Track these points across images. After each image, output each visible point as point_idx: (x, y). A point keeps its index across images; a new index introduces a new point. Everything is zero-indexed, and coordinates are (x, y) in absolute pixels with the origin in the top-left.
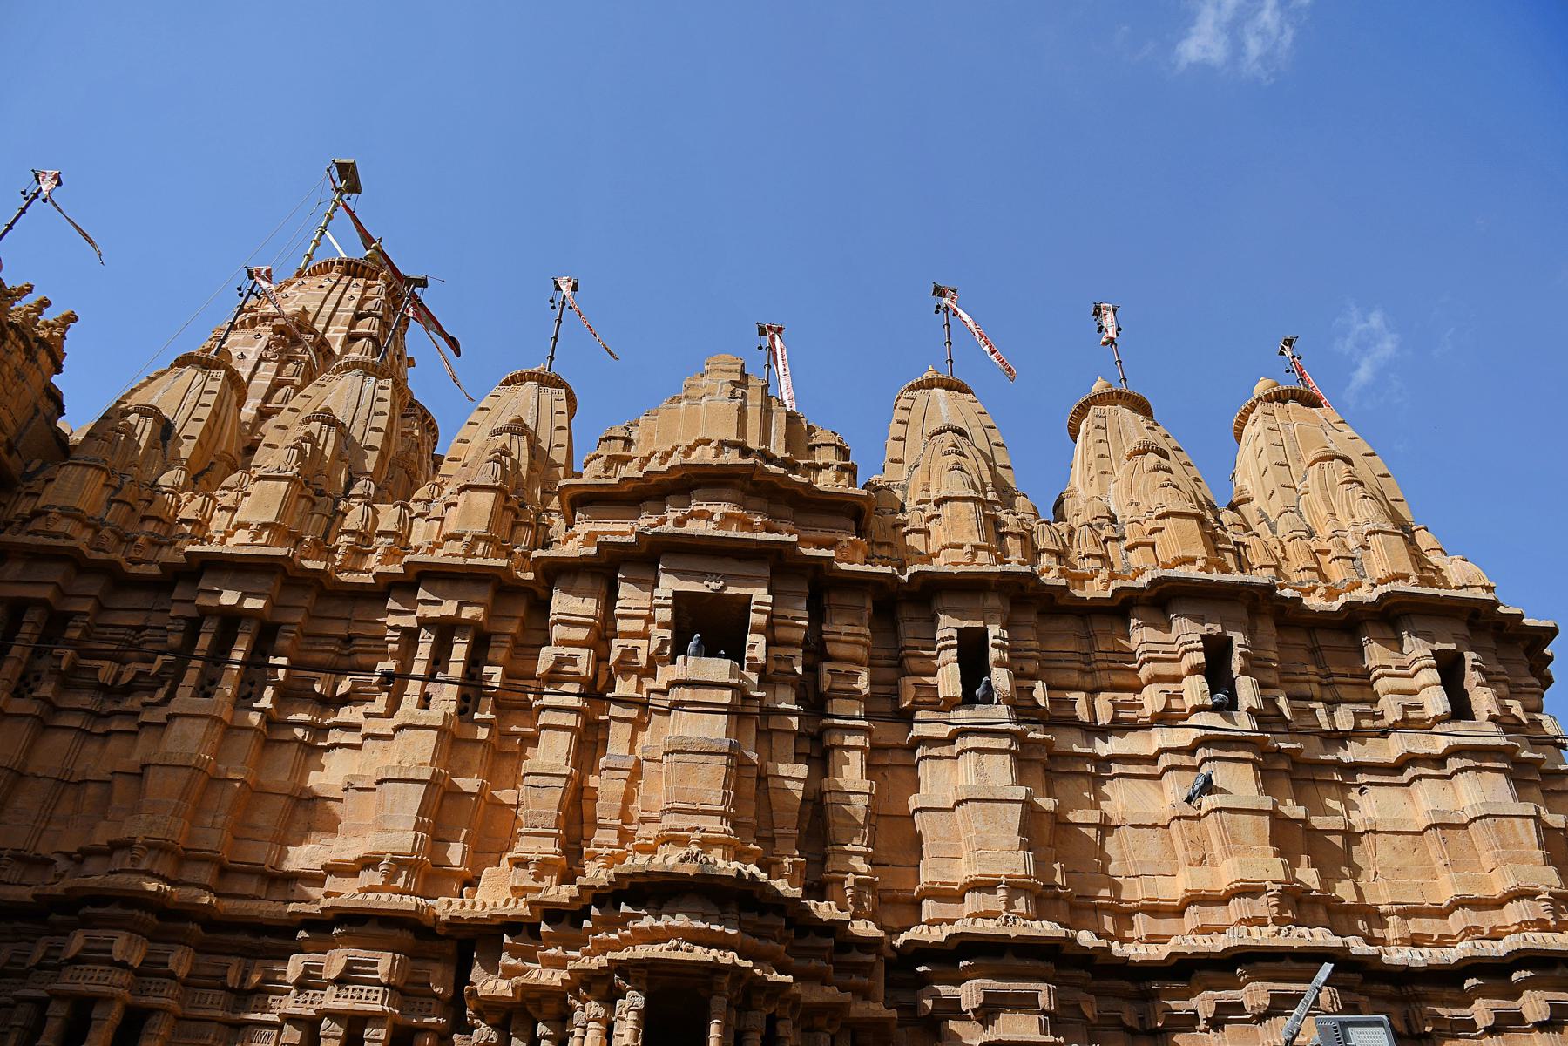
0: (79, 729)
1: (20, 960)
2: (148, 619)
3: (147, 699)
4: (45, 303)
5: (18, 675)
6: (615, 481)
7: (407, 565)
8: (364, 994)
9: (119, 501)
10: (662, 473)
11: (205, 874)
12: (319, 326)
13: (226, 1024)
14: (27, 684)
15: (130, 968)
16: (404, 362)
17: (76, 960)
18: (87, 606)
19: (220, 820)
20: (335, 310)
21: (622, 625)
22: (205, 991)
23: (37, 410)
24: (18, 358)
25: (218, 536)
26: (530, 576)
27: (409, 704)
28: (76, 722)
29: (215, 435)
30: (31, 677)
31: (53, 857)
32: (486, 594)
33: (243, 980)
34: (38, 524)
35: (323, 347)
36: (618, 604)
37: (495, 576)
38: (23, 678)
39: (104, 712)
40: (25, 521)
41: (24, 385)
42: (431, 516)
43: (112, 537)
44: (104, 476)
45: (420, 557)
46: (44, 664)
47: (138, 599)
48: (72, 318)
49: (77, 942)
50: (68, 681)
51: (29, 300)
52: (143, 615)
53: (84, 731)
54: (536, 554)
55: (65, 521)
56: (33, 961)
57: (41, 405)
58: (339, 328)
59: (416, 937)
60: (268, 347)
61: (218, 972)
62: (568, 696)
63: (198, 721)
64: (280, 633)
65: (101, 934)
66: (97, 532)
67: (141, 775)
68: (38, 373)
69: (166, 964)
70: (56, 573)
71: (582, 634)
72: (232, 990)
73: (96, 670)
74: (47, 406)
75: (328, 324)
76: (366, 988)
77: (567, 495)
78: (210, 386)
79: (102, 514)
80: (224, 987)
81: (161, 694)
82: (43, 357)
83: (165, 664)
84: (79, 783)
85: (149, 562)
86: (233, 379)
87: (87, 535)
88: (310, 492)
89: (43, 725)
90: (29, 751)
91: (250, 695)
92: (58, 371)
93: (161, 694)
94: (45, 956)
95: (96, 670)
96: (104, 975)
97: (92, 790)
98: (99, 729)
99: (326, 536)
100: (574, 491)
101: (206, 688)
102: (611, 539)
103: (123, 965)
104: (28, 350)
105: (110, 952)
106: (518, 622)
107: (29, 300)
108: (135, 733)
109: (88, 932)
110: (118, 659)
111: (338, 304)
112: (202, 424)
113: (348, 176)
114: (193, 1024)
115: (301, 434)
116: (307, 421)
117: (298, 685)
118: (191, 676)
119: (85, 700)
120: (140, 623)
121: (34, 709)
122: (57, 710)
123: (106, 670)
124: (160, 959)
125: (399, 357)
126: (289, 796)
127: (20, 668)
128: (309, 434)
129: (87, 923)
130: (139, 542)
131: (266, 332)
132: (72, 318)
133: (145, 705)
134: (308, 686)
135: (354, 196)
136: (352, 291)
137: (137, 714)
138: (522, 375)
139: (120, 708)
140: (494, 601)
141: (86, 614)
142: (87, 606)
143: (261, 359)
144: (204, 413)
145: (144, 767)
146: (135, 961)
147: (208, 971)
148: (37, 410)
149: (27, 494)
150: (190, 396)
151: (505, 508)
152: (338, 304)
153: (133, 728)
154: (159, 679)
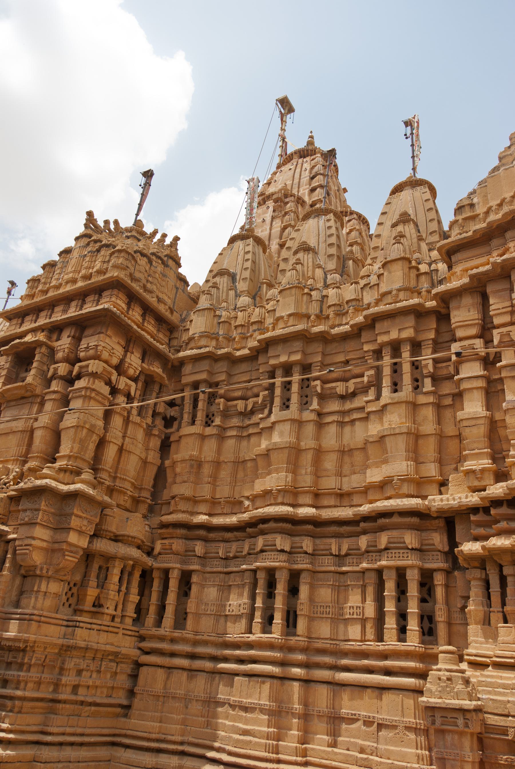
0: (236, 436)
1: (241, 550)
2: (251, 376)
3: (261, 416)
4: (164, 236)
5: (205, 417)
6: (470, 234)
7: (365, 317)
8: (401, 555)
9: (223, 322)
10: (499, 220)
11: (308, 499)
12: (295, 191)
13: (337, 573)
14: (210, 419)
15: (286, 552)
16: (342, 192)
17: (262, 551)
18: (223, 377)
19: (309, 470)
20: (300, 179)
21: (497, 321)
22: (323, 557)
23: (177, 289)
24: (160, 268)
25: (271, 326)
26: (434, 303)
27: (386, 392)
28: (234, 433)
29: (257, 272)
30: (210, 416)
31: (242, 499)
32: (410, 321)
33: (340, 550)
34: (192, 344)
35: (300, 201)
36: (491, 308)
37: (415, 310)
38: (207, 416)
39: (245, 425)
40: (187, 344)
41: (167, 279)
42: (372, 284)
43: (224, 340)
44: (213, 312)
45: (372, 310)
46: (213, 408)
47: (244, 367)
48: (177, 239)
49: (260, 542)
50: (226, 414)
51: (158, 236)
52: (249, 373)
53: (239, 436)
54: (434, 292)
55: (203, 339)
56: (245, 552)
57: (178, 285)
58: (305, 187)
59: (420, 519)
60: (274, 211)
61: (327, 547)
62: (472, 370)
63: (286, 423)
64: (313, 368)
65: (269, 537)
66: (217, 340)
67: (267, 454)
68: (172, 271)
69: (302, 547)
70: (205, 365)
71: (473, 331)
72: (336, 555)
73: (236, 406)
74: (179, 284)
75: (299, 188)
76: (397, 551)
77: (444, 251)
78: (248, 249)
79: (217, 330)
80: (331, 554)
81: (266, 411)
82: (171, 263)
83: (265, 397)
84: (243, 462)
85: (244, 348)
86: (258, 241)
87: (214, 343)
88: (306, 290)
89: (221, 438)
90: (219, 451)
91: (307, 403)
92: (180, 266)
93: (266, 411)
94: (250, 549)
95: (236, 406)
96: (276, 557)
97: (249, 464)
98: (245, 434)
99: (321, 311)
100: (447, 247)
101: (286, 405)
102: (475, 271)
103: (282, 551)
104: (163, 263)
105: (275, 545)
106: (433, 332)
107: (158, 236)
108: (260, 433)
109: (264, 537)
110: (245, 398)
111: (300, 176)
112: (249, 271)
113: (286, 105)
114: (322, 574)
115: (294, 261)
116: (296, 253)
117: (328, 392)
118: (277, 401)
119: (235, 421)
120: (248, 378)
121: (215, 431)
122: (225, 429)
123: (240, 405)
124: (299, 545)
125: (338, 190)
126: (338, 451)
127: (205, 413)
128: (298, 259)
129: (263, 533)
130: (237, 339)
131: (271, 204)
132: (177, 239)
133: (261, 419)
134: (333, 391)
135: (292, 114)
136: (305, 165)
137: (258, 424)
138: (82, 705)
139: (252, 422)
140: (417, 323)
141: (224, 381)
142: (223, 377)
143: (273, 218)
144: (248, 264)
145: (268, 450)
146: (287, 548)
147: (322, 547)
148: (177, 289)
149: (185, 330)
150: (239, 257)
151: (410, 268)
152: (300, 176)
153: (259, 431)
154: (263, 407)
